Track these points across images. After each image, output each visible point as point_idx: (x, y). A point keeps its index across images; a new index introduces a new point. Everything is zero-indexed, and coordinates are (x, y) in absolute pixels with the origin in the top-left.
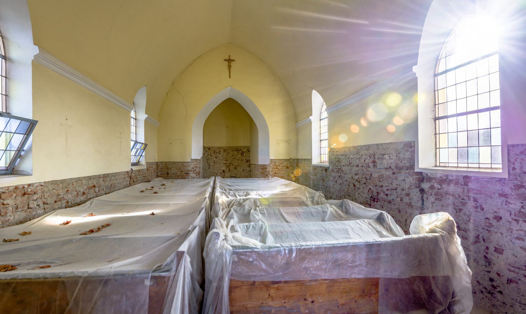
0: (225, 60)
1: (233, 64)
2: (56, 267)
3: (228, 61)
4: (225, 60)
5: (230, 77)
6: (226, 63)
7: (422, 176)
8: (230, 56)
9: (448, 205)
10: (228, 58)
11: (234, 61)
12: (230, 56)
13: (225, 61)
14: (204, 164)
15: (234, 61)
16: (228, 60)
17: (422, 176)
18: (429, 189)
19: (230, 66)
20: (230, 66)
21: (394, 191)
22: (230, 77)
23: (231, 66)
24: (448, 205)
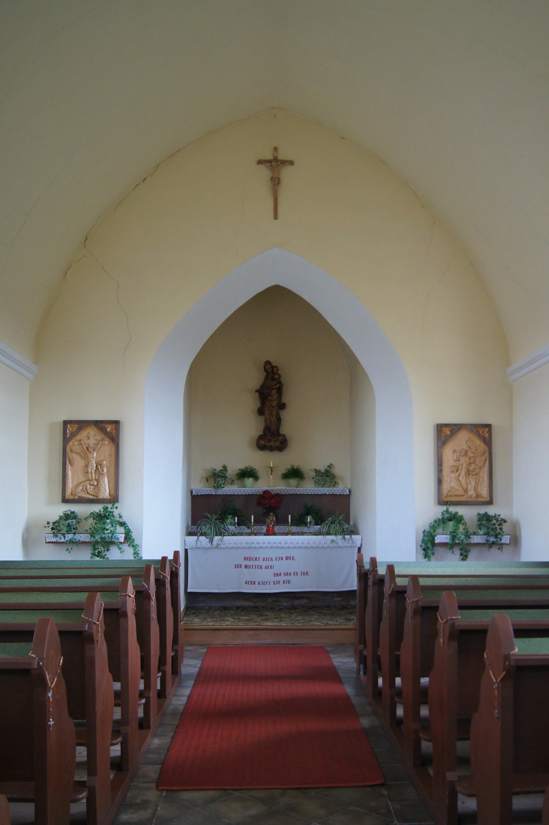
0: (260, 162)
1: (286, 173)
2: (227, 644)
3: (268, 164)
4: (260, 162)
5: (276, 217)
6: (264, 172)
7: (276, 371)
8: (276, 149)
9: (94, 537)
10: (270, 157)
11: (291, 163)
12: (276, 149)
13: (261, 166)
14: (463, 518)
15: (291, 163)
16: (269, 162)
17: (276, 371)
18: (313, 474)
19: (276, 182)
20: (276, 182)
21: (78, 437)
22: (276, 217)
23: (279, 179)
24: (94, 537)
